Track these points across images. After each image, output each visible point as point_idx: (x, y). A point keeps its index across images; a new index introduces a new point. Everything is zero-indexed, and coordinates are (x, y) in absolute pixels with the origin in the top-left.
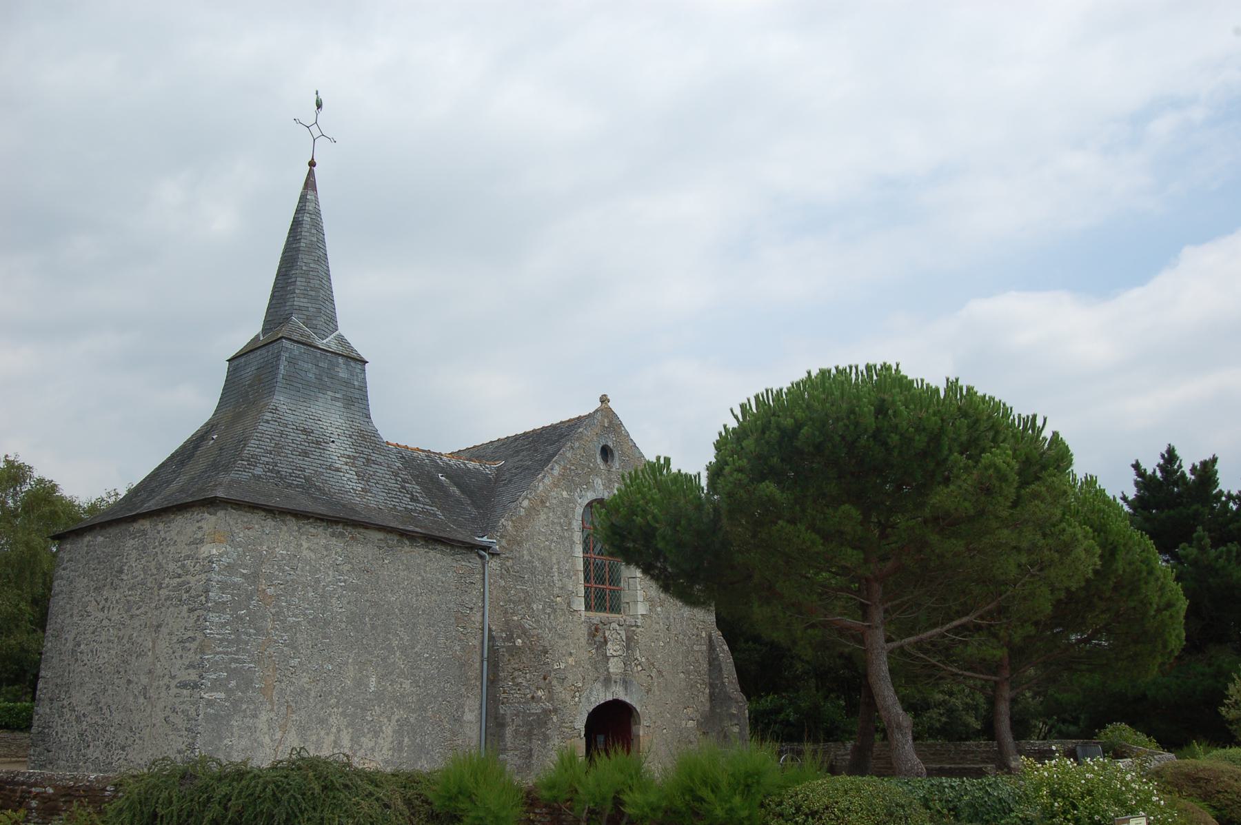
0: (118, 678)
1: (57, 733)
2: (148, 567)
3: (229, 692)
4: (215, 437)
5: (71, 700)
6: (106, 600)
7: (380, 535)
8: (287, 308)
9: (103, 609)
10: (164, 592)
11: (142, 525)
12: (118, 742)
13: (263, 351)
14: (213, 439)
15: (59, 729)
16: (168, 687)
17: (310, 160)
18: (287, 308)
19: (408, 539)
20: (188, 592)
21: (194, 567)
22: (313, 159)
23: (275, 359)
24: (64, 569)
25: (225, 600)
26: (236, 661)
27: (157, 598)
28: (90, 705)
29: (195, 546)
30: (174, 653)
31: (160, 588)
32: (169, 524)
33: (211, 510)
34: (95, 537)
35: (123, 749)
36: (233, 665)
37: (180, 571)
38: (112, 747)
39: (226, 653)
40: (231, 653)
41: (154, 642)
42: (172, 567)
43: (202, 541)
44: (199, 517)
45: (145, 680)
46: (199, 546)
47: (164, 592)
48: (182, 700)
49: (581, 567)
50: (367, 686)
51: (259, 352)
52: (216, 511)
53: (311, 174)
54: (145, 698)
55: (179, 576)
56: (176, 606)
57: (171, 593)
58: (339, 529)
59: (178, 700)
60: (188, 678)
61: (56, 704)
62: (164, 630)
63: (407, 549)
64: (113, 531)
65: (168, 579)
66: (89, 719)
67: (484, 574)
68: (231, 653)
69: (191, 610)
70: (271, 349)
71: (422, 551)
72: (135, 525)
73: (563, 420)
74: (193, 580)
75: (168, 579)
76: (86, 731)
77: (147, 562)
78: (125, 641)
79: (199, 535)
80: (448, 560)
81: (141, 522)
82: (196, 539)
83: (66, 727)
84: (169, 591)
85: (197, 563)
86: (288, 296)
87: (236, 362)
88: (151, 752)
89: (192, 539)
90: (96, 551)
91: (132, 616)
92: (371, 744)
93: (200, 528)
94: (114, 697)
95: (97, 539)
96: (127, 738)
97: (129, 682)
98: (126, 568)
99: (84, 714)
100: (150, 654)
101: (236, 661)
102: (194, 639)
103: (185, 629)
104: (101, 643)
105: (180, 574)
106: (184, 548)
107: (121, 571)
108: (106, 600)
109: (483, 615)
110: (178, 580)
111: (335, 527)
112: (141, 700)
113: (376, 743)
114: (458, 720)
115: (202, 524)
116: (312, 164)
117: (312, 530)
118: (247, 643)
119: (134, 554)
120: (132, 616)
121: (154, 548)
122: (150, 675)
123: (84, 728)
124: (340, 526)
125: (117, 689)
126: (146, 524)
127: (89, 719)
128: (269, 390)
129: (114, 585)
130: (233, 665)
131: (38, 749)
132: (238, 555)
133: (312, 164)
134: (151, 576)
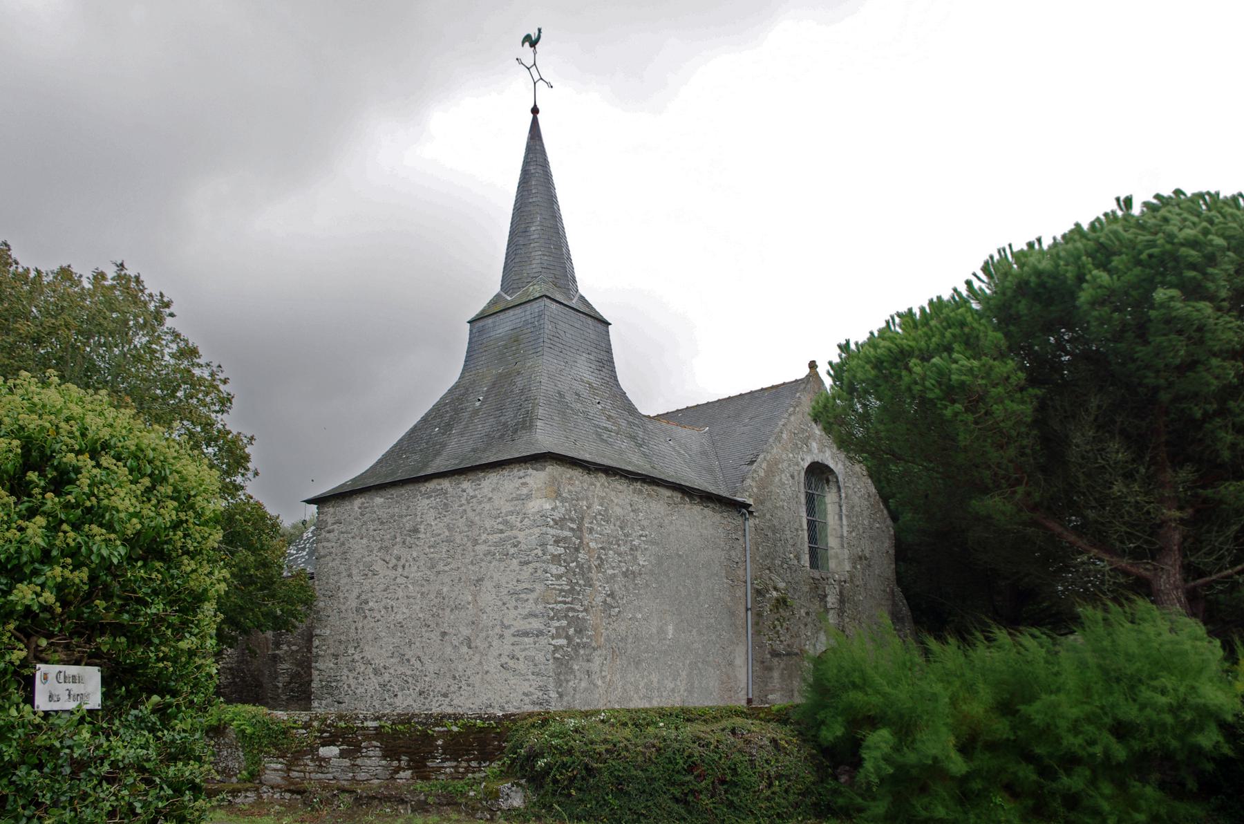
0: (426, 631)
1: (349, 686)
2: (454, 525)
3: (568, 637)
4: (481, 398)
5: (364, 654)
6: (399, 558)
7: (668, 493)
8: (534, 266)
9: (395, 568)
10: (481, 548)
11: (439, 484)
12: (436, 690)
13: (518, 311)
14: (479, 400)
15: (352, 682)
16: (501, 636)
17: (532, 105)
18: (534, 266)
19: (688, 497)
20: (515, 546)
21: (521, 522)
22: (535, 105)
23: (537, 319)
24: (329, 532)
25: (559, 552)
26: (573, 610)
27: (472, 554)
28: (392, 657)
29: (521, 502)
30: (504, 604)
31: (475, 543)
32: (478, 482)
33: (538, 466)
34: (372, 499)
35: (445, 695)
36: (571, 614)
37: (501, 527)
38: (429, 695)
39: (565, 603)
40: (568, 603)
41: (474, 596)
42: (488, 523)
43: (529, 497)
44: (521, 473)
45: (466, 632)
46: (525, 502)
47: (481, 548)
48: (522, 647)
49: (805, 527)
50: (666, 634)
51: (511, 312)
52: (545, 467)
53: (535, 125)
54: (470, 647)
55: (502, 532)
56: (500, 560)
57: (493, 548)
58: (638, 485)
59: (517, 648)
60: (528, 627)
61: (342, 660)
62: (488, 584)
63: (688, 506)
64: (395, 492)
65: (485, 535)
66: (392, 671)
67: (745, 530)
68: (568, 603)
69: (523, 564)
70: (529, 308)
71: (698, 508)
72: (427, 484)
73: (764, 387)
74: (521, 536)
75: (485, 535)
76: (389, 682)
77: (452, 520)
78: (432, 596)
79: (525, 491)
80: (718, 517)
81: (441, 481)
82: (520, 495)
83: (361, 679)
84: (490, 546)
85: (525, 518)
86: (533, 254)
87: (480, 324)
88: (485, 697)
89: (514, 495)
90: (375, 512)
91: (439, 573)
92: (672, 686)
93: (524, 484)
94: (425, 649)
95: (375, 501)
96: (449, 686)
97: (444, 634)
98: (422, 527)
99: (385, 668)
100: (470, 607)
101: (573, 610)
102: (532, 591)
103: (518, 581)
104: (398, 599)
105: (501, 530)
106: (504, 505)
107: (416, 531)
108: (399, 558)
109: (746, 569)
110: (500, 535)
111: (635, 484)
112: (464, 649)
113: (676, 685)
114: (731, 664)
115: (527, 480)
116: (535, 111)
117: (619, 487)
118: (579, 594)
119: (432, 513)
120: (439, 573)
121: (461, 506)
122: (473, 627)
123: (387, 679)
124: (639, 484)
125: (428, 641)
126: (446, 484)
127: (392, 671)
128: (533, 351)
129: (407, 543)
130: (571, 614)
131: (324, 702)
132: (566, 510)
133: (535, 111)
134: (460, 533)
